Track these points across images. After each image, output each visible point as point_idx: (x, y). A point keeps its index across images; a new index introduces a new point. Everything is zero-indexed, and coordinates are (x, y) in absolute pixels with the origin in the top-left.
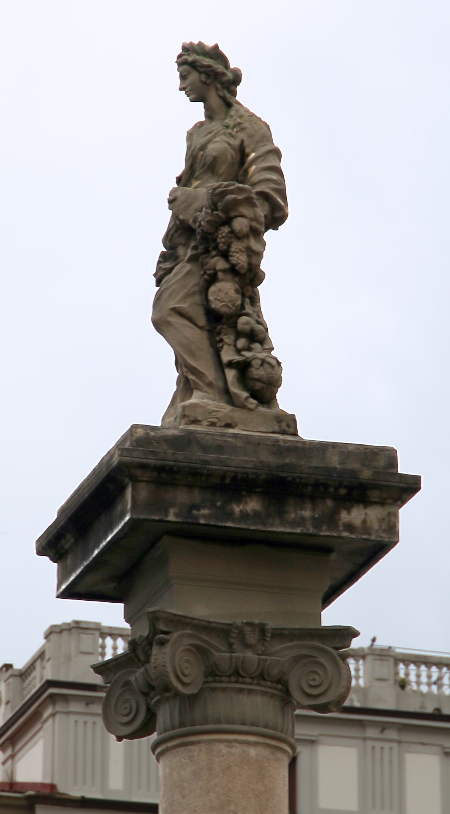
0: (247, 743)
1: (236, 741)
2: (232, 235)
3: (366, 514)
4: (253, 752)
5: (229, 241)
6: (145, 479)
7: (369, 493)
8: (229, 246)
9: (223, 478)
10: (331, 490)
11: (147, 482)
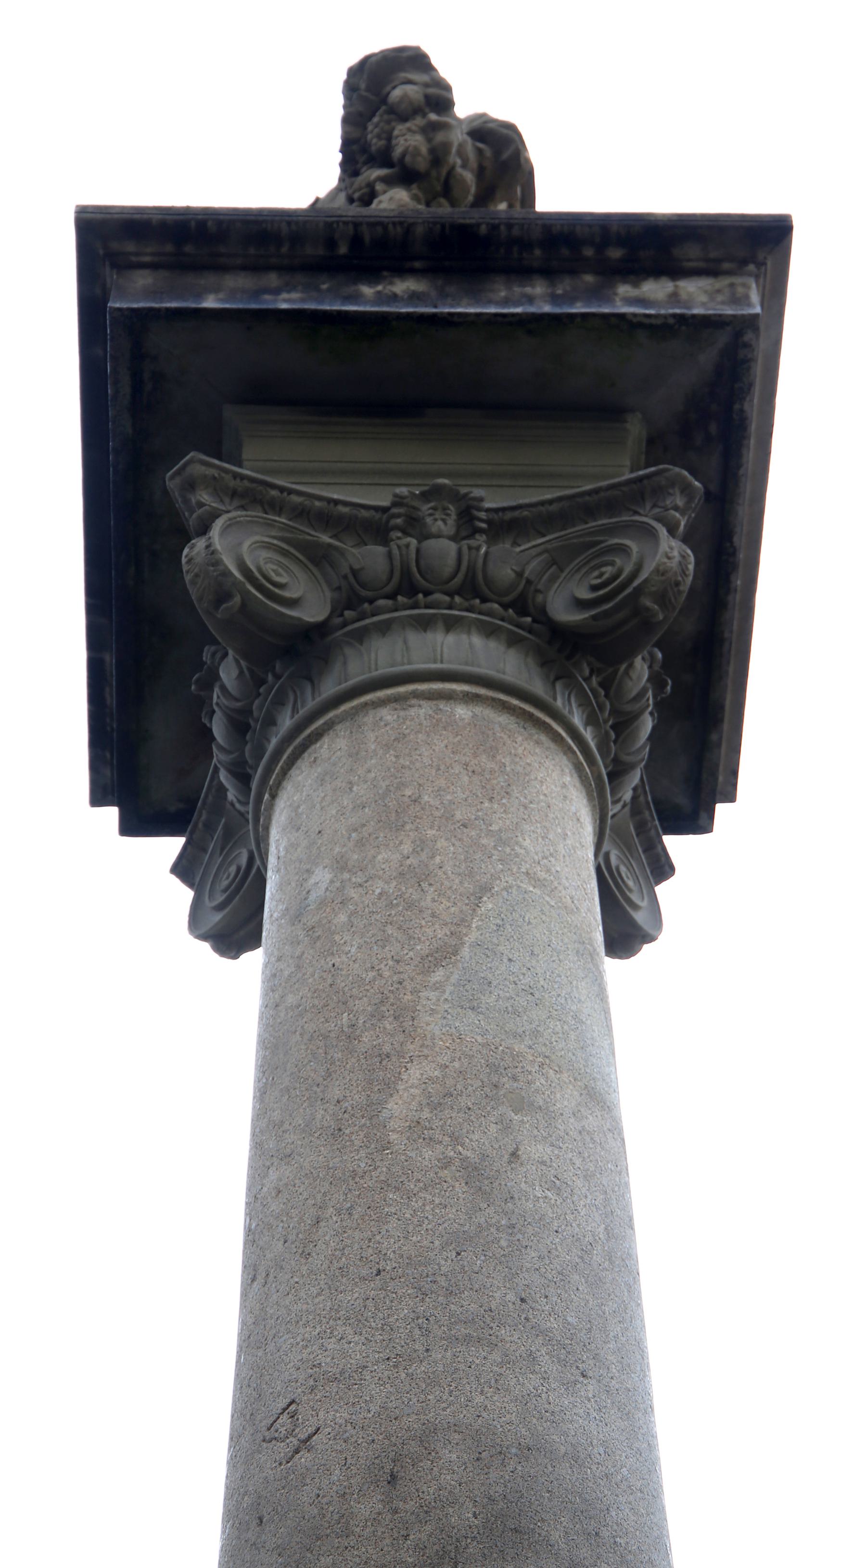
0: (449, 697)
1: (416, 695)
2: (392, 116)
3: (676, 287)
4: (462, 712)
5: (387, 127)
6: (147, 259)
7: (677, 252)
8: (389, 138)
9: (331, 243)
10: (589, 252)
11: (154, 266)
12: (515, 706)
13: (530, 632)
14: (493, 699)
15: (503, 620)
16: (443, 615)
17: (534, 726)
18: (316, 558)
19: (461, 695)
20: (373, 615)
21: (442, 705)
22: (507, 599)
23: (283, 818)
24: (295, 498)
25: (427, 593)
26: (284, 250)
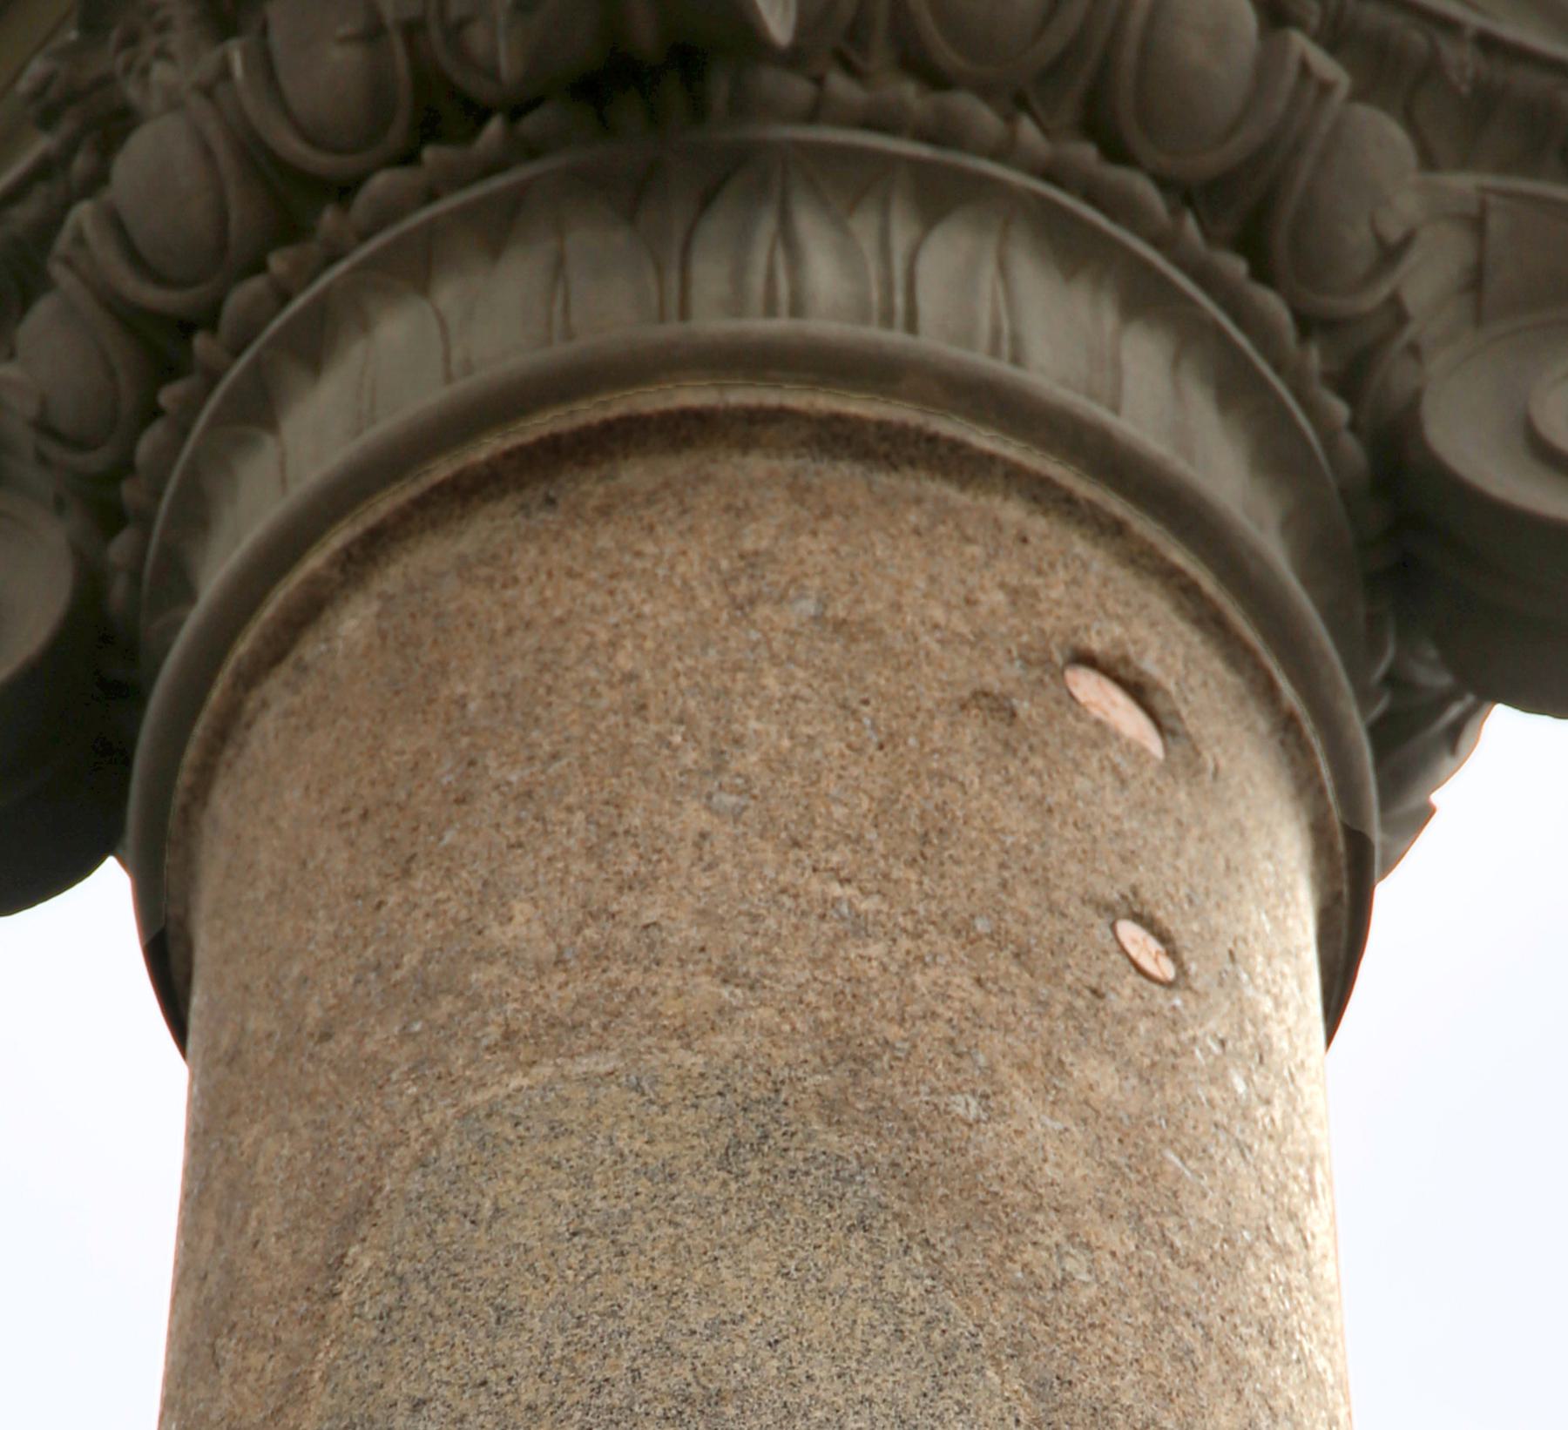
12: (488, 463)
15: (432, 196)
16: (273, 342)
17: (585, 464)
19: (336, 574)
22: (397, 135)
23: (688, 1221)
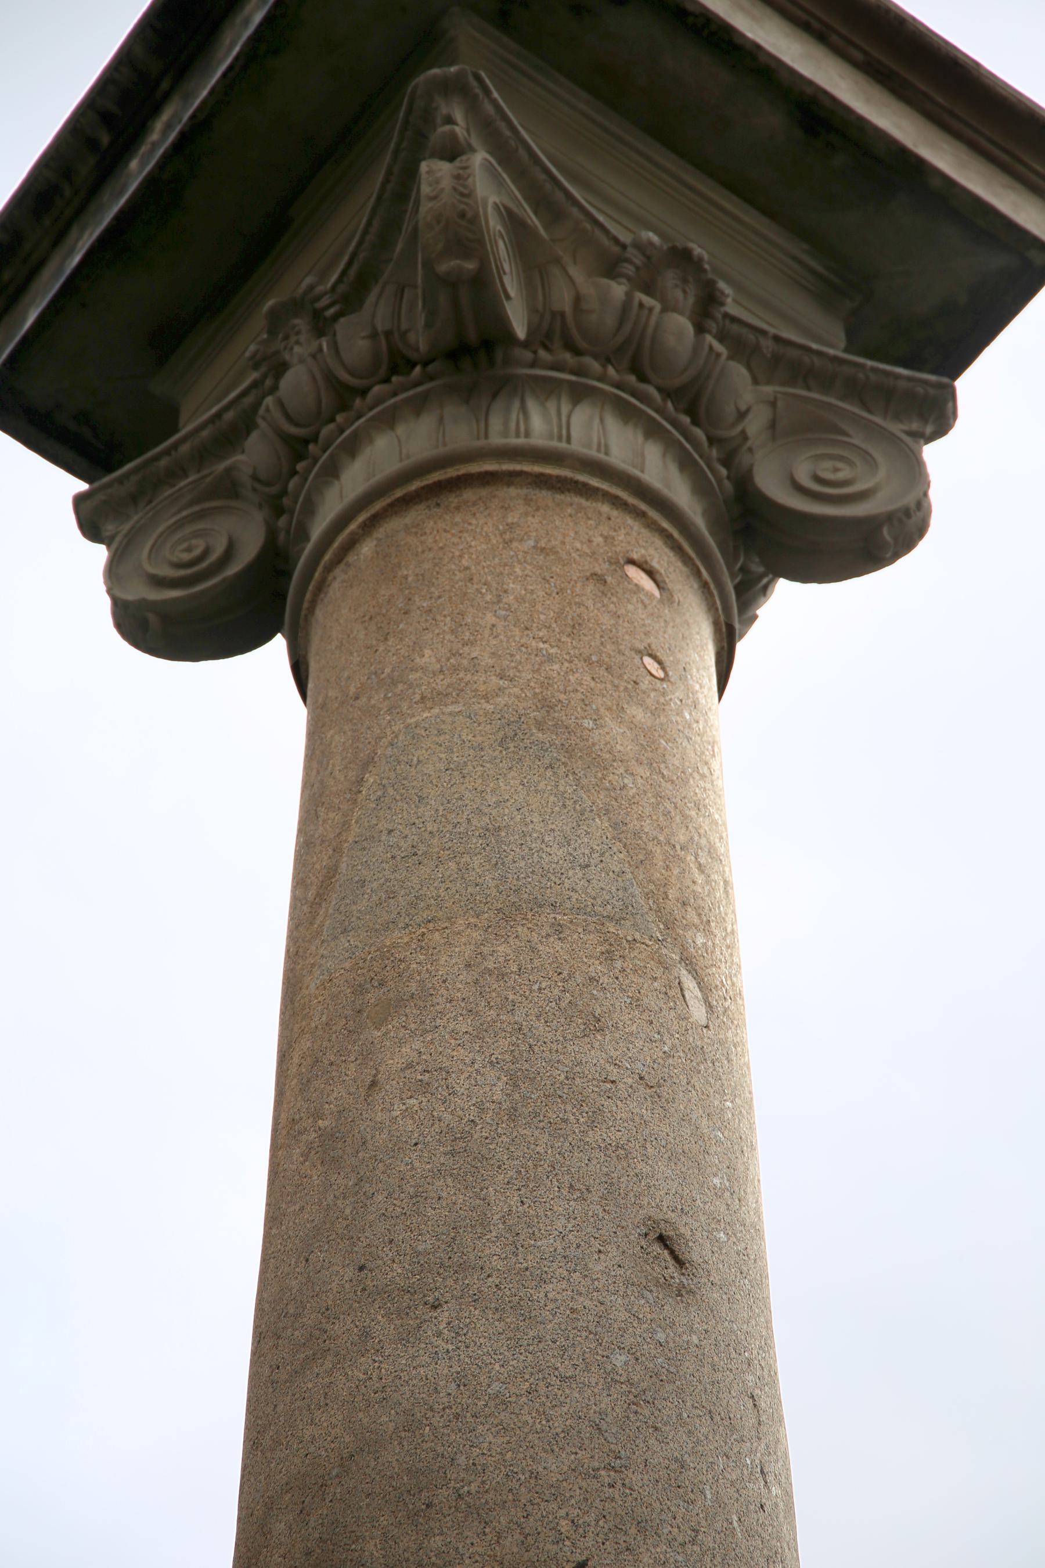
9: (92, 144)
12: (415, 491)
13: (431, 379)
14: (391, 505)
15: (395, 394)
18: (227, 489)
19: (360, 531)
20: (296, 503)
21: (351, 558)
22: (382, 372)
24: (185, 448)
25: (315, 438)
26: (68, 192)
